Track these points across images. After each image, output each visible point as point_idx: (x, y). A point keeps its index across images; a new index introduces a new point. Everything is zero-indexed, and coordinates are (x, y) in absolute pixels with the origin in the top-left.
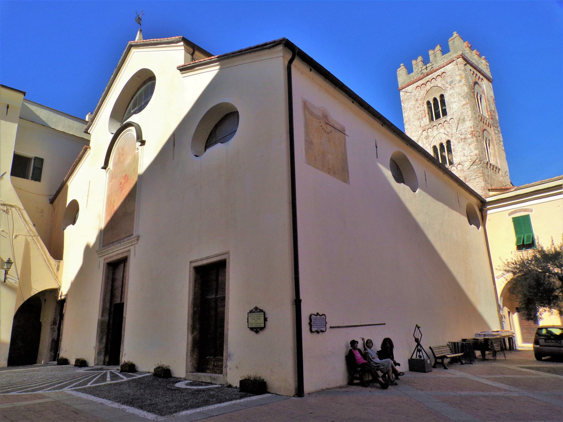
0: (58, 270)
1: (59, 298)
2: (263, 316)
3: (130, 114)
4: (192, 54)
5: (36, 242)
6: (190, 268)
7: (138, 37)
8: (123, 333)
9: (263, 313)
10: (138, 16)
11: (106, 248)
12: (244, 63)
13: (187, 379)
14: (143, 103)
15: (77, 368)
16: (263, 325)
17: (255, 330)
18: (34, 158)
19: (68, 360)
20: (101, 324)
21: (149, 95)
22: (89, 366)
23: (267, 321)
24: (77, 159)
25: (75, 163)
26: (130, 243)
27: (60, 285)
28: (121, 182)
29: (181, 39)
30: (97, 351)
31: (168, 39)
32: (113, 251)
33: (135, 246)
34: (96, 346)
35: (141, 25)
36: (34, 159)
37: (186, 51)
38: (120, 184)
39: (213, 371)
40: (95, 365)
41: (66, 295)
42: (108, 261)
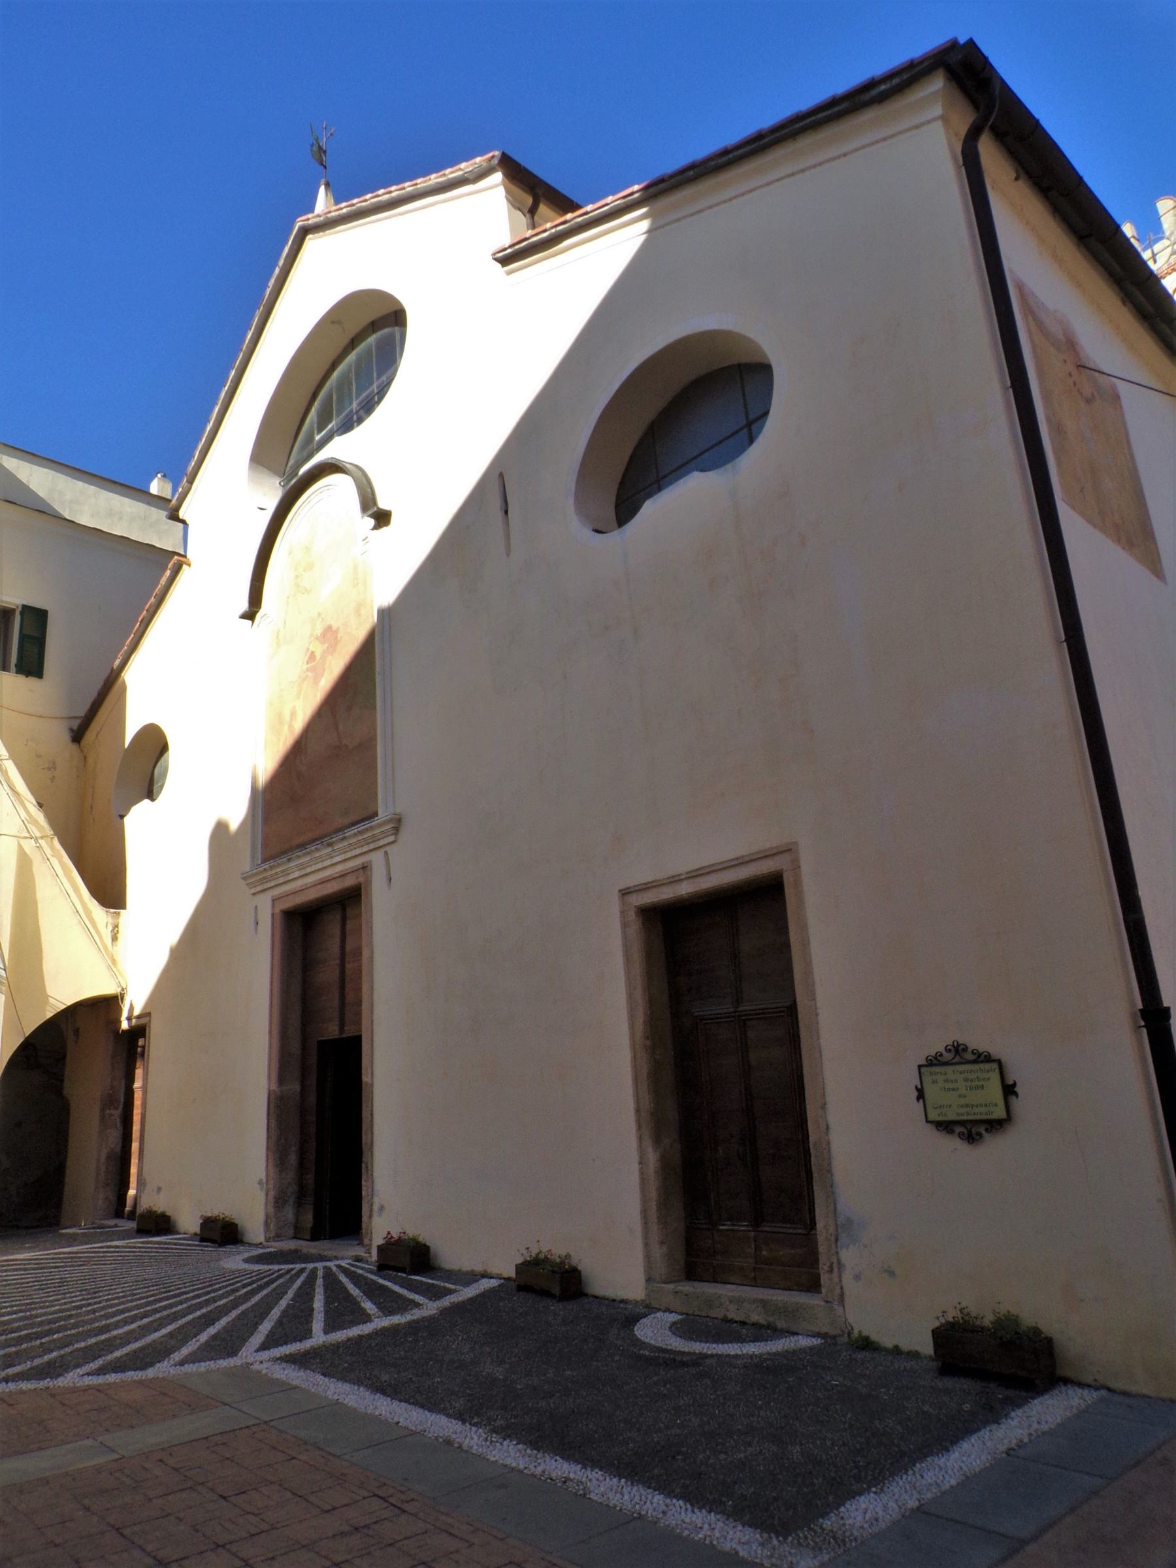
0: (115, 938)
1: (125, 1025)
2: (995, 1078)
3: (310, 447)
4: (532, 211)
5: (49, 856)
6: (622, 912)
7: (323, 203)
8: (365, 1139)
9: (995, 1066)
10: (317, 140)
11: (279, 865)
12: (775, 177)
13: (654, 1304)
14: (355, 405)
15: (210, 1248)
16: (999, 1113)
17: (958, 1129)
18: (20, 609)
19: (169, 1217)
20: (278, 1107)
21: (375, 375)
22: (245, 1240)
23: (1016, 1094)
24: (152, 600)
25: (145, 612)
26: (368, 844)
27: (124, 987)
28: (313, 652)
29: (496, 161)
30: (272, 1193)
31: (444, 175)
32: (303, 872)
33: (386, 852)
34: (267, 1176)
35: (325, 167)
36: (22, 613)
37: (514, 203)
38: (310, 658)
39: (755, 1278)
40: (267, 1240)
41: (145, 1014)
42: (288, 904)
